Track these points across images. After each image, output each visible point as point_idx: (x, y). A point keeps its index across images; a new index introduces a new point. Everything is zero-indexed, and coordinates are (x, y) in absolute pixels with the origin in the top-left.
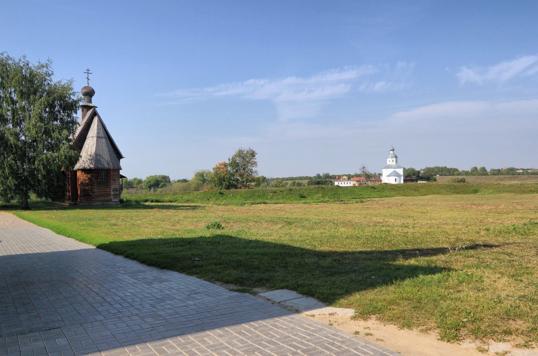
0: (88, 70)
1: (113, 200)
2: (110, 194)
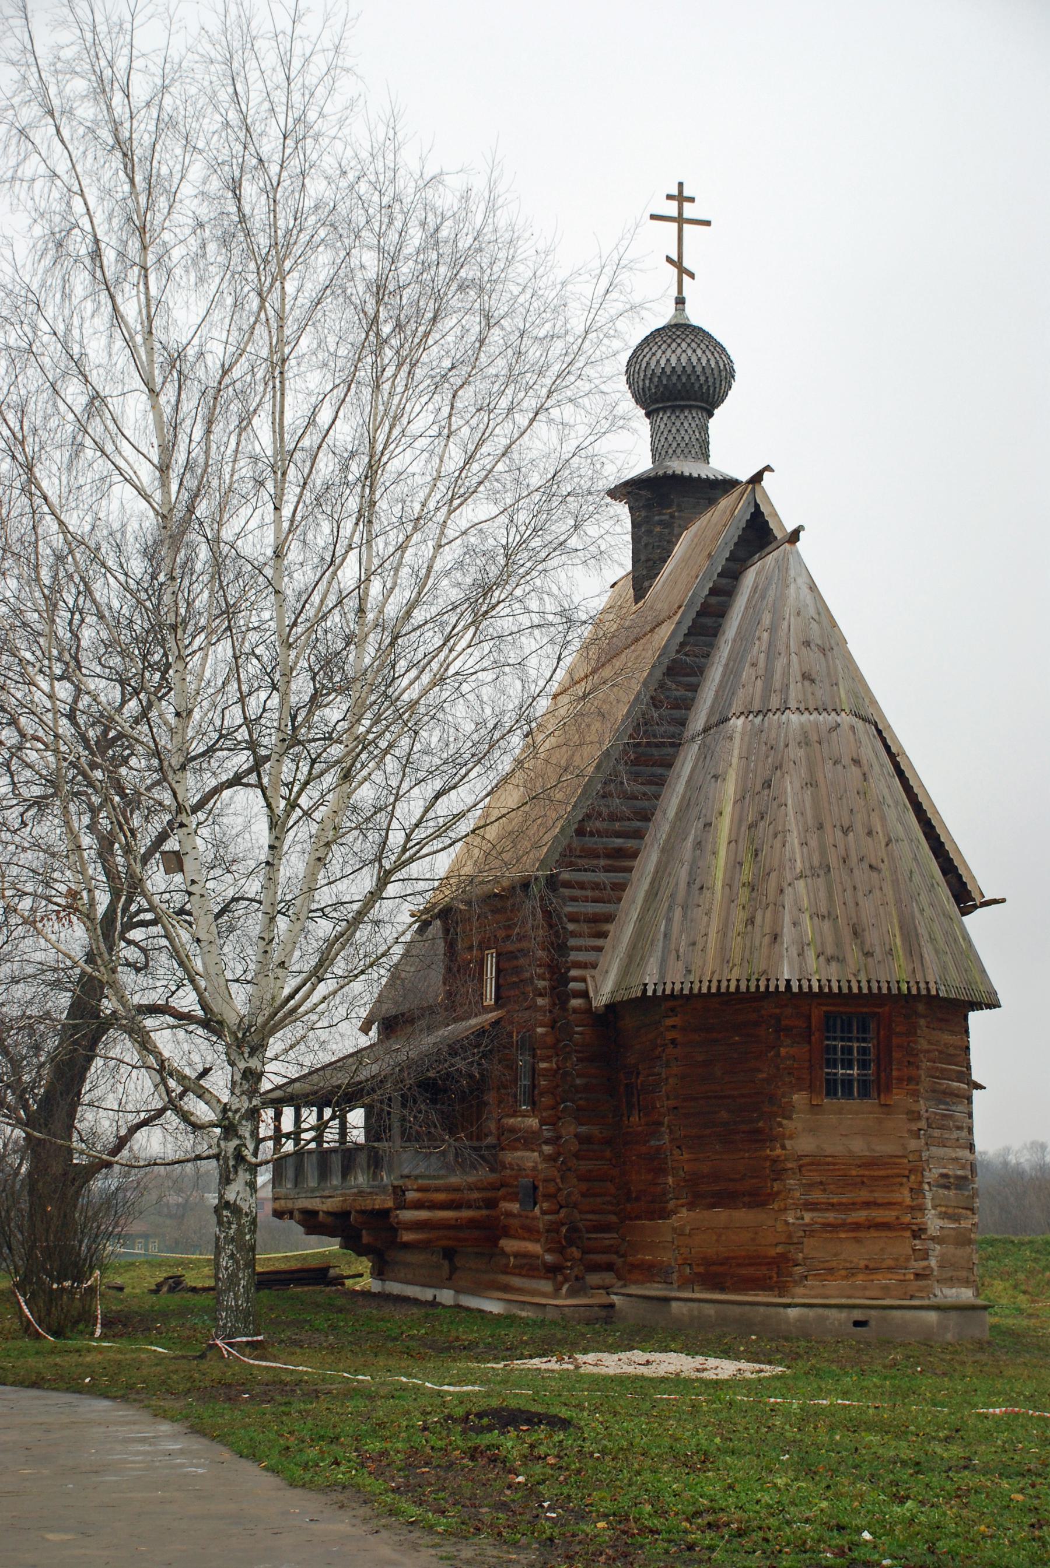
0: (680, 198)
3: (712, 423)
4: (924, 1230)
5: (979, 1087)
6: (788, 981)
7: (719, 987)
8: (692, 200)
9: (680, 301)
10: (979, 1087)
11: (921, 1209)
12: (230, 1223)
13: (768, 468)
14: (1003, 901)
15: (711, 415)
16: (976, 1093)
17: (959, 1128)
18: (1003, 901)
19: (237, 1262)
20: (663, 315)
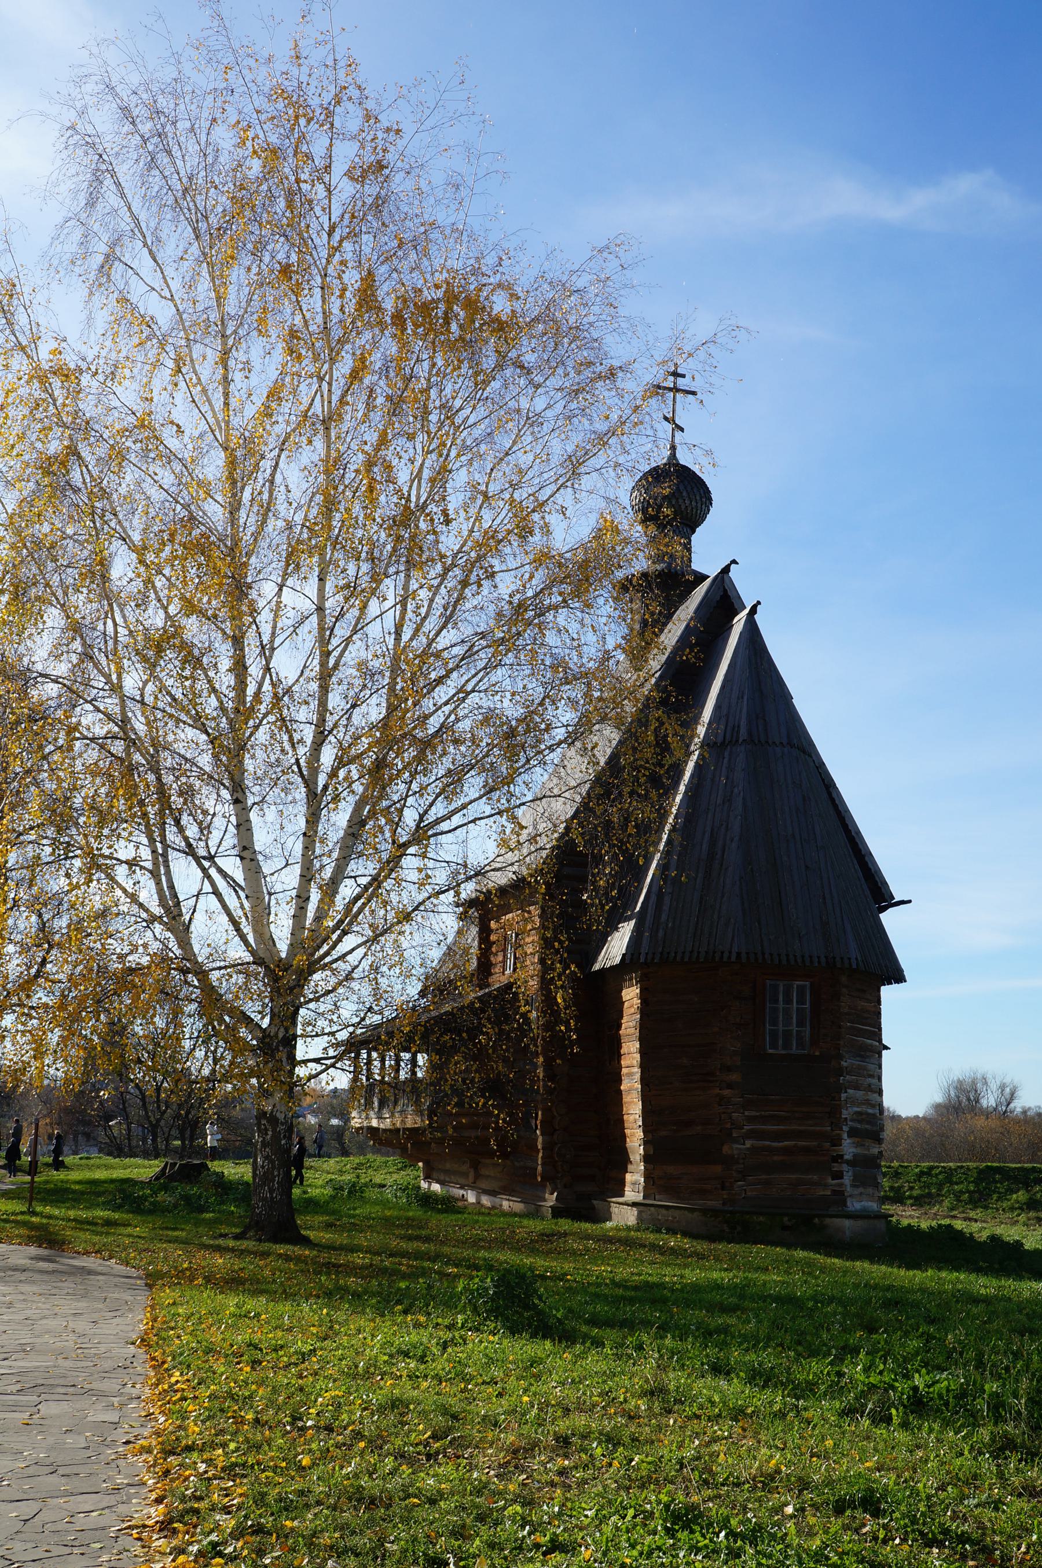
1: (855, 1205)
2: (839, 1158)
3: (694, 538)
4: (842, 1156)
5: (886, 1048)
6: (739, 954)
7: (683, 958)
8: (683, 376)
9: (673, 448)
10: (886, 1048)
11: (837, 1142)
12: (266, 1130)
13: (734, 562)
14: (910, 902)
15: (694, 532)
16: (884, 1052)
17: (872, 1076)
18: (910, 902)
19: (272, 1162)
20: (660, 458)
